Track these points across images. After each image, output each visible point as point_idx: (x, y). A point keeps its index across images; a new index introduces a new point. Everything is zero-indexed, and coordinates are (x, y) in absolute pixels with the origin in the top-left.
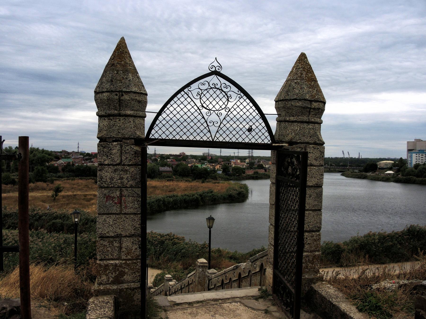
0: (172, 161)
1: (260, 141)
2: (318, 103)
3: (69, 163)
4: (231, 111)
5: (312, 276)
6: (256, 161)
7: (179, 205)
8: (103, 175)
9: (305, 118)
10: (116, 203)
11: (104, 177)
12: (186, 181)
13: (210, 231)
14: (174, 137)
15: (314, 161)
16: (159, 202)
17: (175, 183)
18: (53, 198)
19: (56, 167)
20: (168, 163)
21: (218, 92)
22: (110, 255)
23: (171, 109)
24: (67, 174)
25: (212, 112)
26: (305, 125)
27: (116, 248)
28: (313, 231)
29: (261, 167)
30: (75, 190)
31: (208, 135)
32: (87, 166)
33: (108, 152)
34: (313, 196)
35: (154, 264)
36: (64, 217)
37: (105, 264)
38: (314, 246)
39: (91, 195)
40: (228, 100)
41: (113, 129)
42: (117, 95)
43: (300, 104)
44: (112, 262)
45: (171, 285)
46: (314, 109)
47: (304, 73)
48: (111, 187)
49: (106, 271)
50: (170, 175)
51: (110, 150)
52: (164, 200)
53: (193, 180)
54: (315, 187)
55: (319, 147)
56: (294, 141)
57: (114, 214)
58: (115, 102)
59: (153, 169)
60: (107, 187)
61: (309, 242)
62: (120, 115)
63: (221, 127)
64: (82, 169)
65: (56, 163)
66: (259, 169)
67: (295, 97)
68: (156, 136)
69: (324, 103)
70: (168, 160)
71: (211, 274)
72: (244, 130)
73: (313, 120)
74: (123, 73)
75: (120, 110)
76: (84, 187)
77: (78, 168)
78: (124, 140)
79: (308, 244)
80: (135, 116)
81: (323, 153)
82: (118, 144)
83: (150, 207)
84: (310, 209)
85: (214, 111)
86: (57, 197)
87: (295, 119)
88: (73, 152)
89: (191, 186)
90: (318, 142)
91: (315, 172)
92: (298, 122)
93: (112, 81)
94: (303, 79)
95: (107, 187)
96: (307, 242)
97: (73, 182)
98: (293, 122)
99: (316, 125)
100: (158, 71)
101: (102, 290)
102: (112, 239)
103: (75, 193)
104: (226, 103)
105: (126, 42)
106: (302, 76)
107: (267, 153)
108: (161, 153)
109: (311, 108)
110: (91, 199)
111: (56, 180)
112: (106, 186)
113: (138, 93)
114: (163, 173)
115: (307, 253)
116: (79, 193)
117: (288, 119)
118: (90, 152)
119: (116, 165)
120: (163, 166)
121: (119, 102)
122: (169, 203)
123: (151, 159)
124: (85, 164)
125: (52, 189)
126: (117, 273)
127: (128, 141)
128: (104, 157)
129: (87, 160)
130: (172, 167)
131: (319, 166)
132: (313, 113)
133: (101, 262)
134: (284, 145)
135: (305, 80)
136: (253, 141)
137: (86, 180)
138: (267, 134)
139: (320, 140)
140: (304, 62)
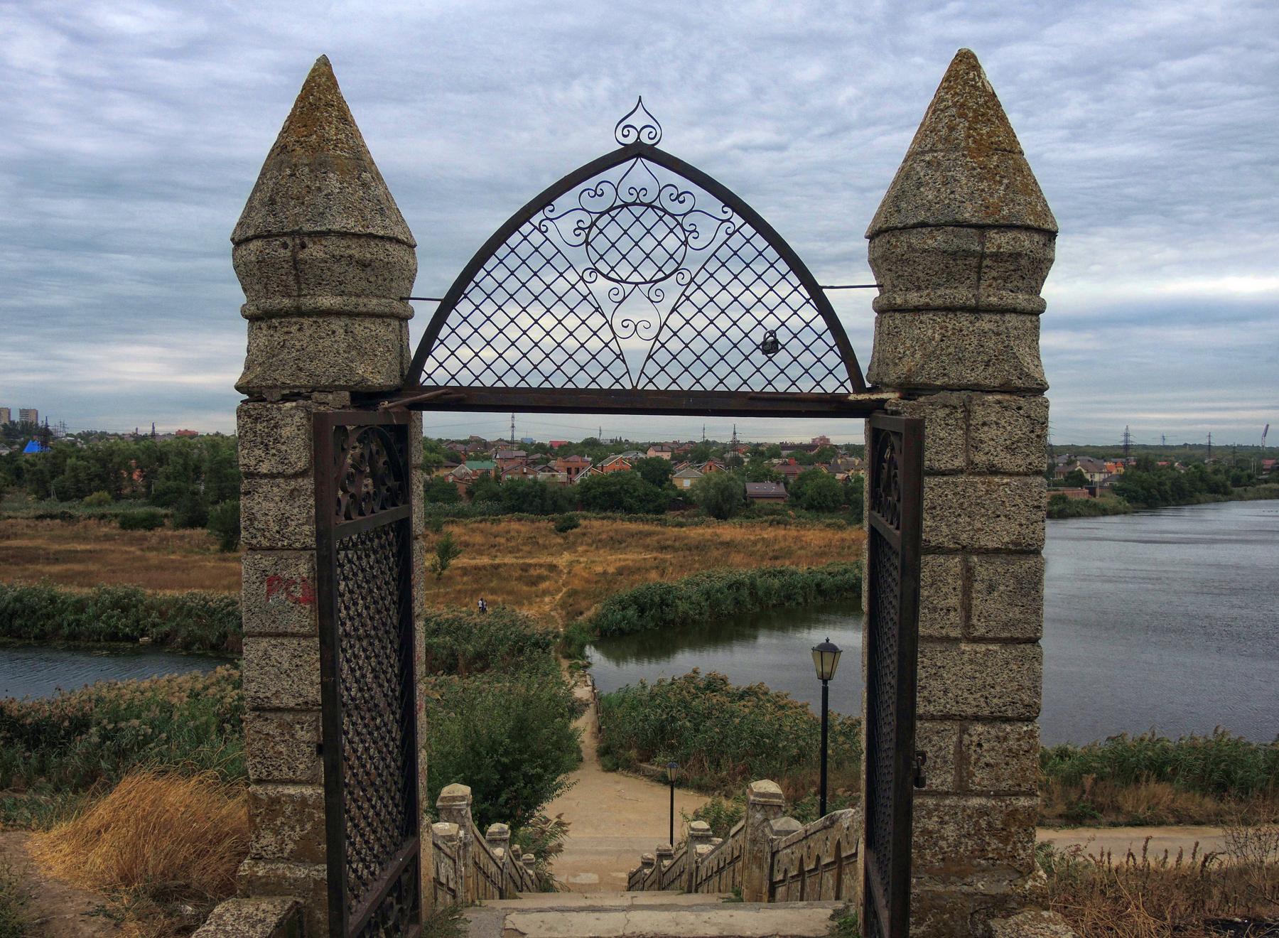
0: (785, 464)
1: (806, 386)
2: (1010, 235)
3: (488, 472)
4: (699, 280)
5: (1004, 887)
6: (1061, 461)
7: (801, 600)
8: (256, 508)
9: (962, 294)
10: (297, 601)
11: (259, 516)
12: (828, 526)
13: (825, 691)
14: (500, 379)
15: (1002, 454)
16: (738, 589)
17: (793, 532)
18: (435, 575)
19: (449, 484)
20: (775, 469)
21: (650, 218)
22: (285, 769)
23: (488, 284)
24: (482, 506)
25: (628, 288)
26: (964, 320)
27: (304, 746)
28: (1007, 720)
29: (1077, 480)
30: (498, 551)
31: (618, 369)
32: (535, 481)
33: (269, 435)
34: (1002, 588)
35: (706, 780)
36: (458, 629)
37: (270, 797)
38: (1012, 776)
39: (541, 566)
40: (685, 243)
41: (280, 357)
42: (285, 246)
43: (937, 240)
44: (291, 790)
45: (701, 855)
46: (996, 257)
47: (963, 125)
48: (283, 548)
49: (273, 820)
50: (779, 507)
51: (275, 427)
52: (751, 584)
53: (850, 524)
54: (1009, 552)
55: (1022, 402)
56: (920, 380)
57: (293, 635)
58: (283, 271)
59: (726, 488)
60: (271, 549)
61: (988, 760)
62: (300, 313)
63: (662, 338)
64: (520, 489)
65: (448, 475)
66: (1071, 485)
67: (922, 216)
68: (441, 378)
69: (1051, 235)
70: (775, 461)
71: (778, 833)
72: (747, 346)
73: (994, 300)
74: (311, 171)
75: (299, 296)
76: (524, 544)
77: (170, 482)
78: (316, 394)
79: (987, 765)
80: (352, 315)
81: (868, 423)
82: (297, 408)
83: (711, 606)
84: (991, 635)
85: (637, 284)
86: (446, 572)
87: (923, 301)
88: (501, 440)
89: (843, 540)
90: (1019, 383)
91: (1007, 496)
92: (937, 309)
93: (272, 202)
94: (956, 148)
95: (271, 549)
96: (983, 760)
97: (495, 528)
98: (917, 310)
99: (1007, 317)
100: (438, 163)
101: (261, 878)
102: (289, 717)
103: (497, 561)
104: (678, 257)
105: (336, 70)
106: (954, 134)
107: (849, 432)
108: (755, 441)
109: (983, 256)
110: (541, 578)
111: (448, 523)
112: (265, 543)
113: (357, 236)
114: (757, 501)
115: (983, 801)
116: (509, 560)
117: (899, 301)
118: (547, 442)
119: (296, 476)
120: (757, 479)
121: (296, 269)
122: (768, 592)
123: (723, 459)
124: (531, 477)
125: (433, 548)
126: (308, 826)
127: (330, 397)
128: (257, 452)
129: (535, 463)
130: (786, 484)
131: (1026, 474)
132: (994, 274)
133: (259, 790)
134: (884, 396)
135: (964, 148)
136: (781, 385)
137: (533, 521)
138: (832, 359)
139: (1028, 375)
140: (966, 83)
